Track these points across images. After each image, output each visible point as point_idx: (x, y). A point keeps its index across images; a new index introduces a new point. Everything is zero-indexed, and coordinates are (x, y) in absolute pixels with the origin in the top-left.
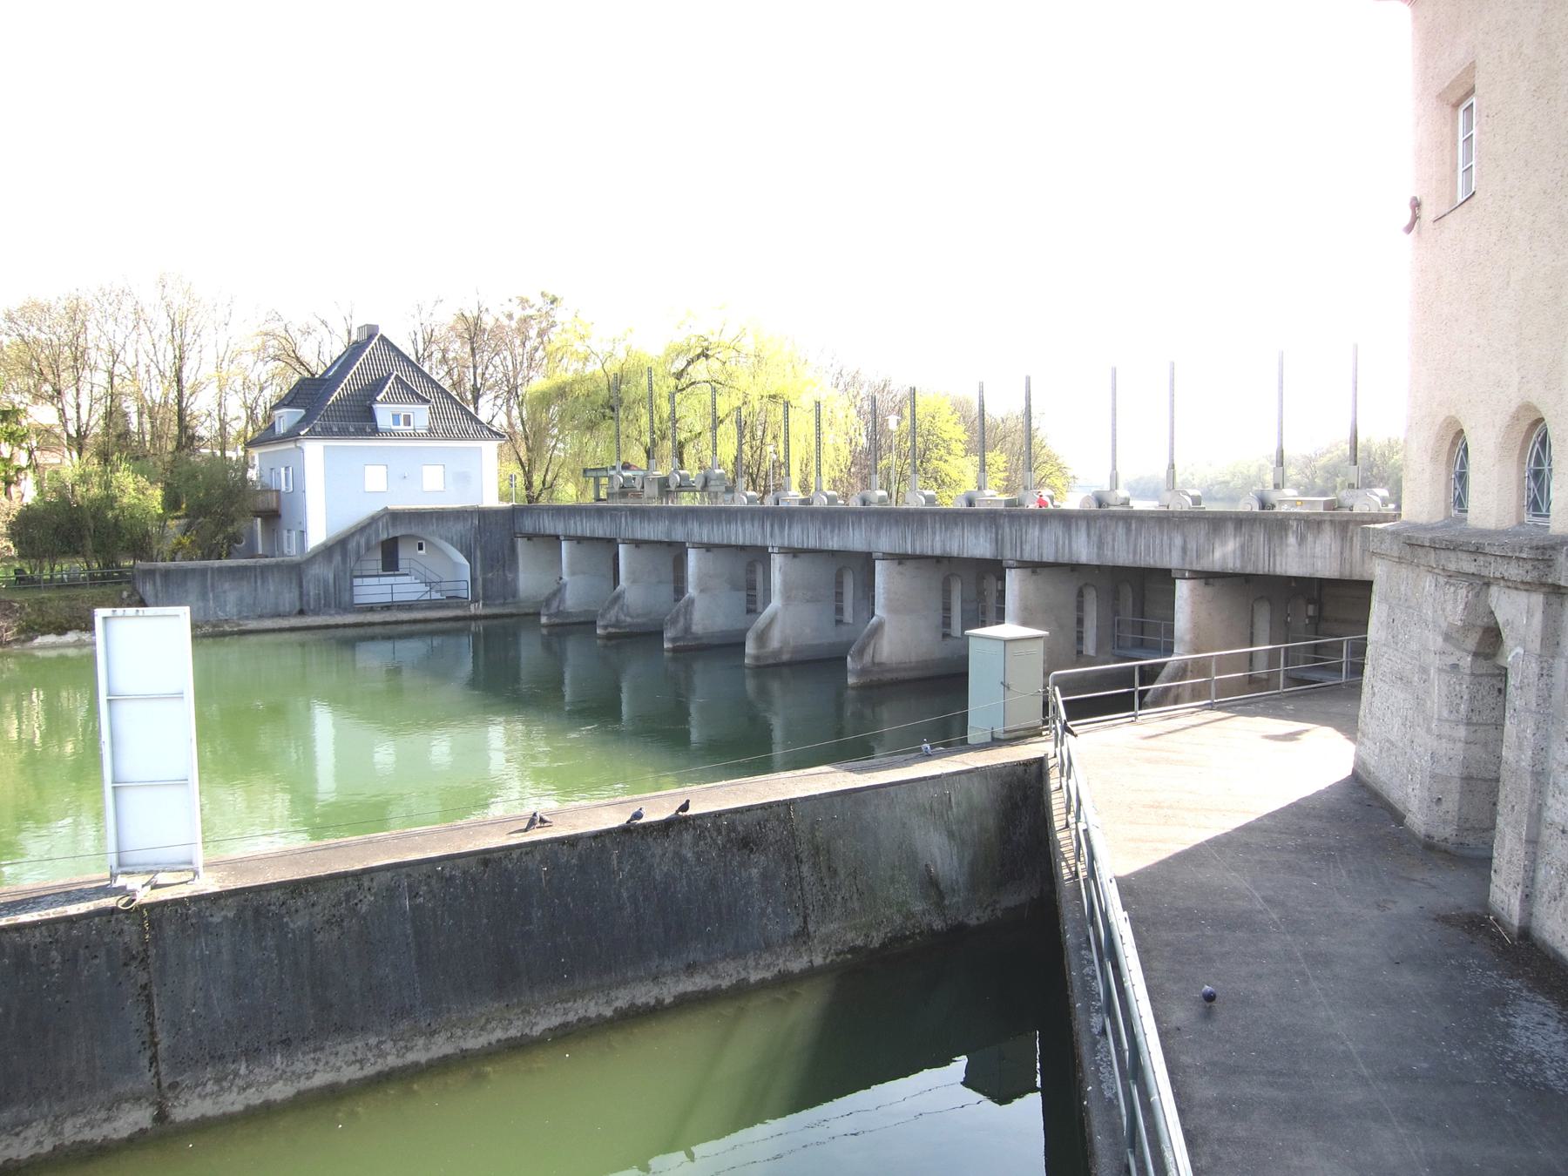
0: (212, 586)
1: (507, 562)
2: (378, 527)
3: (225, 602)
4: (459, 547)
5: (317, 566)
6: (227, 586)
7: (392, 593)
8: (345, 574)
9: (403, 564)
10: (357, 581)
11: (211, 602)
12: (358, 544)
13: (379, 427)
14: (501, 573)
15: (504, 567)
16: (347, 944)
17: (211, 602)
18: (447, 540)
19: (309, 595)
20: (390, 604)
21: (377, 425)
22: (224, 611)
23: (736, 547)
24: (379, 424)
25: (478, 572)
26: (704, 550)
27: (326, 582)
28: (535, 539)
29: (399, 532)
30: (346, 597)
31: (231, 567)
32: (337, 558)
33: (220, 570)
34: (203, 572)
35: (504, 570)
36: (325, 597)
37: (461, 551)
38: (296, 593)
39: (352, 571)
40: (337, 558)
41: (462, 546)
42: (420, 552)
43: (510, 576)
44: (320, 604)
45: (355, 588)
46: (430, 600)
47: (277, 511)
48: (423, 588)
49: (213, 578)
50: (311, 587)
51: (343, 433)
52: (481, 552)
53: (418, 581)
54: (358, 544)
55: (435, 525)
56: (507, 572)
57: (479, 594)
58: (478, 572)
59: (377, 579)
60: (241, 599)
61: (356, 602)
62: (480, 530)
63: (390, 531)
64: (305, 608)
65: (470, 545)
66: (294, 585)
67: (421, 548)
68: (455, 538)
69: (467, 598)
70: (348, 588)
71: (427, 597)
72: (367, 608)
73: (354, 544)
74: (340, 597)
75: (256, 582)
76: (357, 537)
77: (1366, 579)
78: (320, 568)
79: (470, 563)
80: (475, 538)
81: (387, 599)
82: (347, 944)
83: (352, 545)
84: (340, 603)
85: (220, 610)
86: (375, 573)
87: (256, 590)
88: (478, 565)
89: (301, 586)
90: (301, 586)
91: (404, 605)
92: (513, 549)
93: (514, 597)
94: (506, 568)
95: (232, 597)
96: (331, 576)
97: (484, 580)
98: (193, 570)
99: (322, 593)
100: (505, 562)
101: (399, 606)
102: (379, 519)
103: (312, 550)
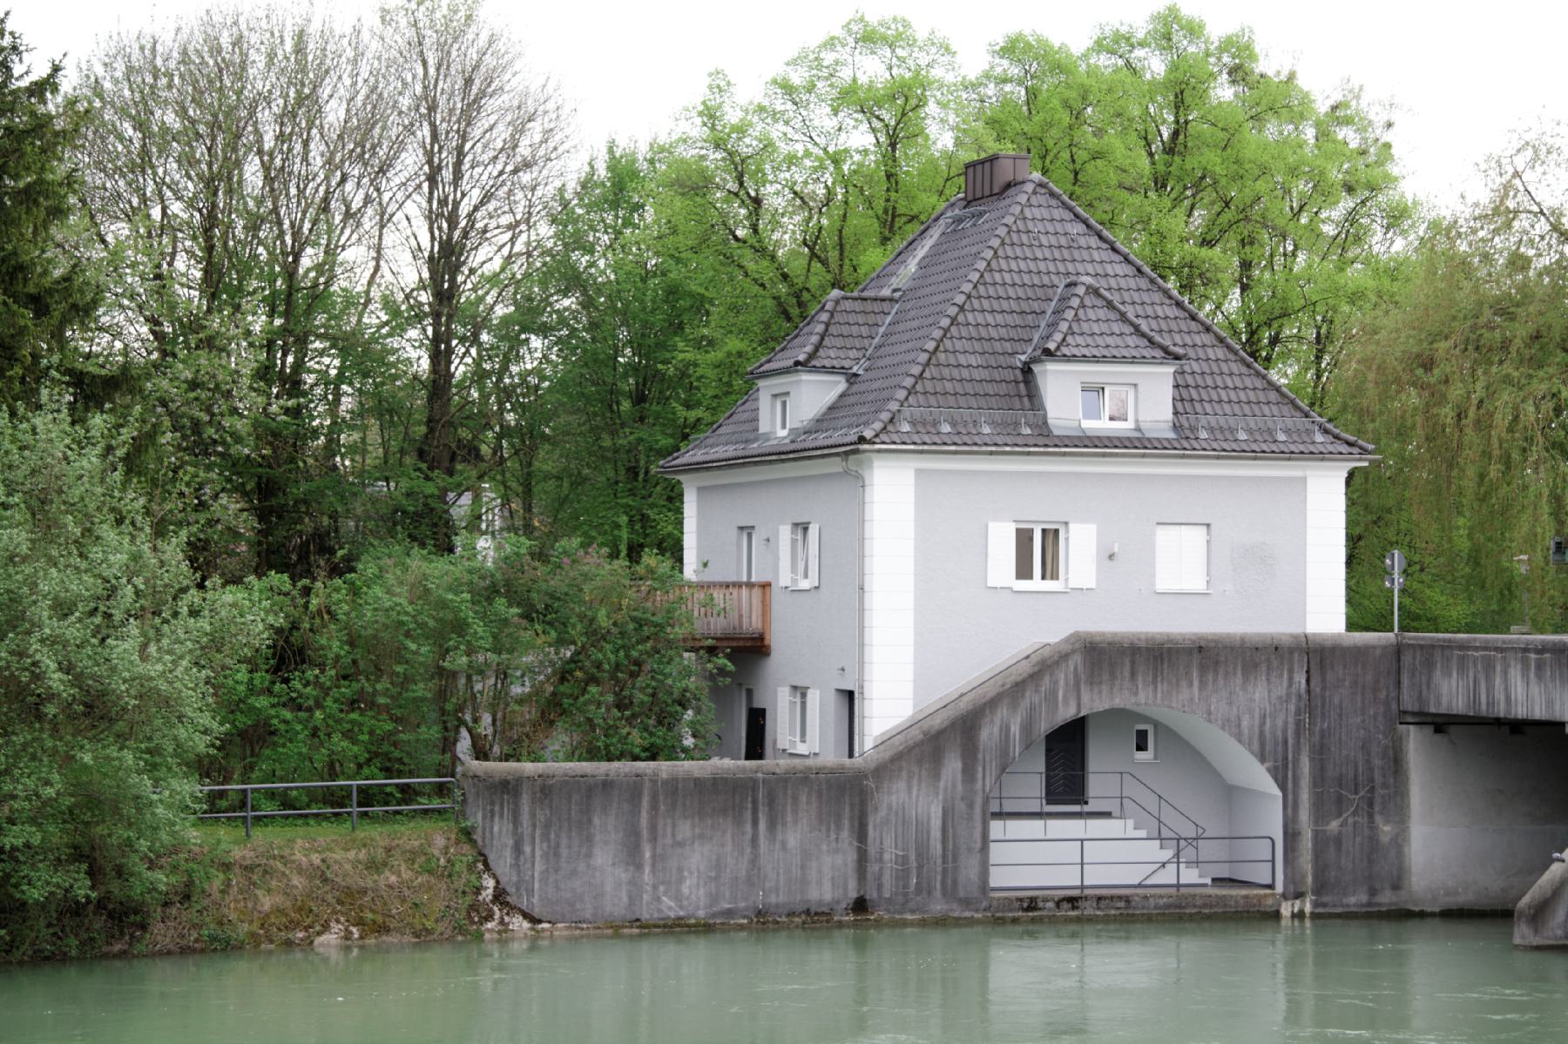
0: (653, 829)
1: (1380, 791)
2: (1056, 683)
3: (680, 870)
4: (1256, 746)
5: (901, 785)
6: (685, 829)
7: (1082, 864)
8: (971, 806)
9: (1099, 784)
10: (996, 828)
11: (647, 870)
12: (1005, 730)
13: (1050, 421)
14: (1362, 820)
15: (1371, 804)
16: (566, 302)
17: (647, 870)
18: (1226, 724)
19: (881, 860)
20: (1076, 893)
21: (1045, 416)
22: (678, 898)
23: (1498, 722)
24: (1050, 415)
25: (1304, 815)
26: (1429, 730)
27: (923, 830)
28: (1452, 729)
29: (1093, 702)
30: (969, 870)
31: (698, 782)
32: (953, 765)
33: (673, 788)
34: (634, 788)
35: (1371, 816)
36: (920, 867)
37: (1262, 759)
38: (847, 857)
39: (986, 800)
40: (953, 765)
41: (1262, 744)
42: (1140, 755)
43: (1386, 830)
44: (906, 886)
45: (992, 845)
46: (1178, 886)
47: (761, 638)
48: (1154, 851)
49: (654, 807)
50: (888, 842)
51: (965, 443)
52: (1312, 760)
53: (1143, 833)
54: (1005, 730)
55: (1196, 683)
56: (1378, 819)
57: (1304, 877)
58: (1304, 815)
59: (1038, 824)
60: (718, 865)
61: (993, 883)
62: (1311, 704)
63: (1085, 697)
64: (871, 894)
65: (1285, 742)
66: (845, 834)
67: (1141, 747)
68: (1245, 723)
69: (1271, 887)
70: (978, 845)
71: (1167, 877)
72: (1021, 900)
73: (996, 730)
74: (956, 868)
75: (755, 822)
76: (1002, 712)
77: (1558, 719)
78: (910, 788)
79: (1283, 788)
80: (1298, 723)
81: (1067, 878)
82: (566, 302)
83: (988, 734)
84: (955, 882)
85: (665, 894)
86: (1035, 806)
87: (754, 841)
88: (1305, 796)
89: (861, 835)
90: (861, 835)
91: (1112, 898)
92: (1397, 764)
93: (1396, 887)
94: (1377, 808)
95: (697, 858)
96: (936, 813)
97: (1318, 837)
98: (607, 785)
99: (913, 857)
100: (1372, 790)
101: (1099, 898)
102: (1057, 663)
103: (880, 745)
